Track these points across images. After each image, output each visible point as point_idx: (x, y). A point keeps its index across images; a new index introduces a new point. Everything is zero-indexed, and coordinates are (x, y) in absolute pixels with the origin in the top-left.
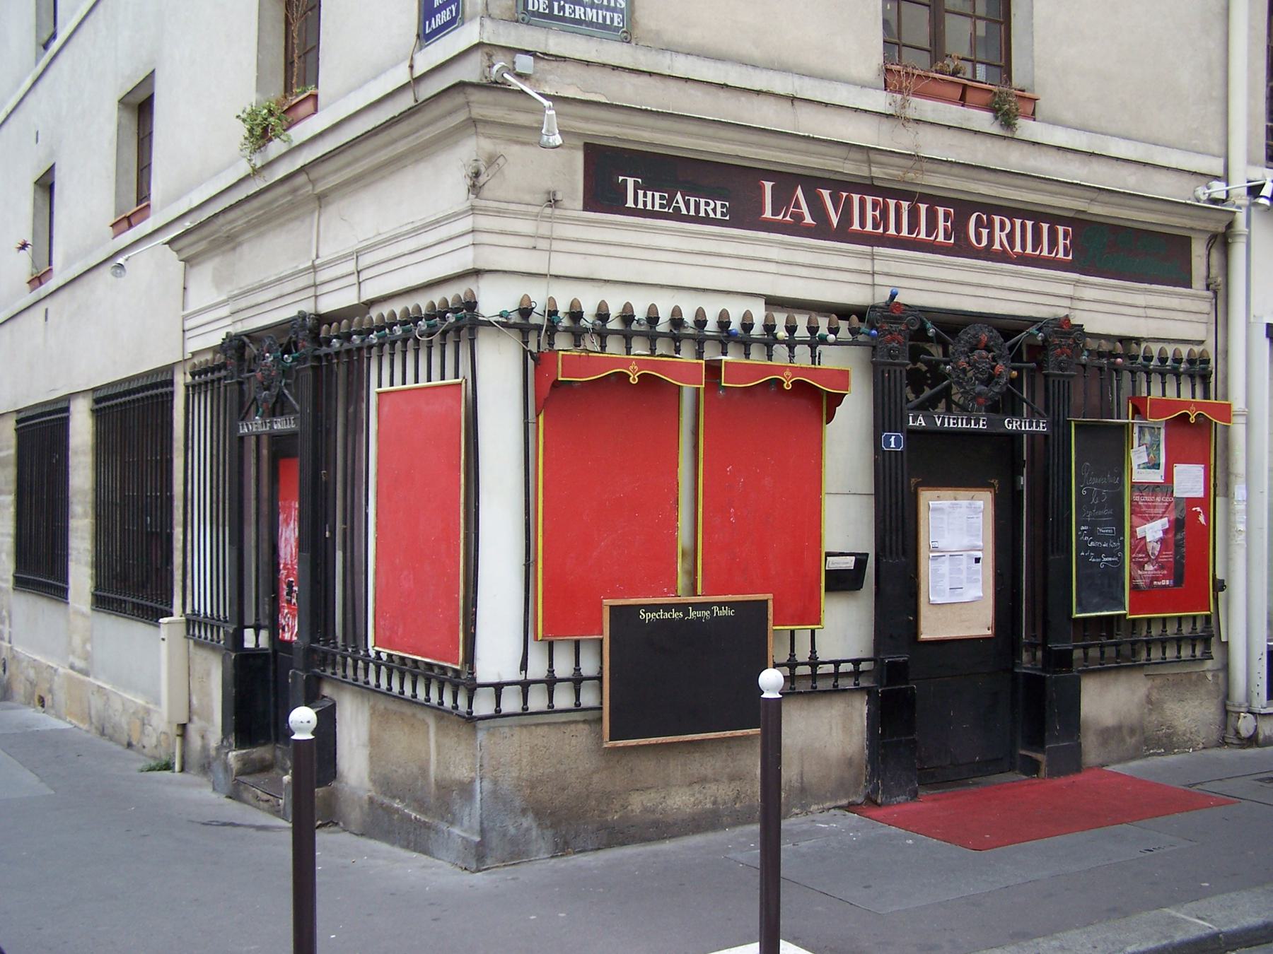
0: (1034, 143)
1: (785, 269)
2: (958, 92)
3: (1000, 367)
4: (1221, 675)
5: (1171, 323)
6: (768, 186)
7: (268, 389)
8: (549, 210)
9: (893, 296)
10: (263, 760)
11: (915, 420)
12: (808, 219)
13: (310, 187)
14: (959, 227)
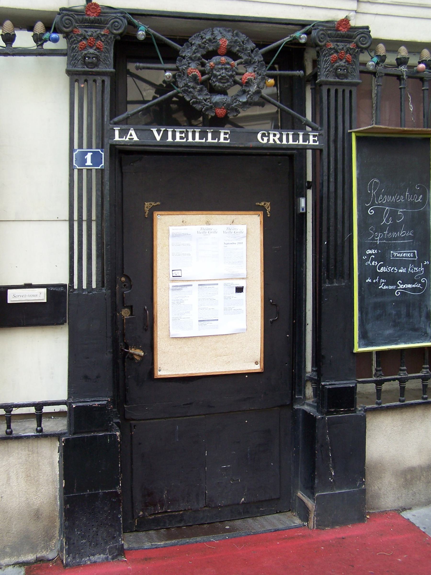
11: (123, 133)
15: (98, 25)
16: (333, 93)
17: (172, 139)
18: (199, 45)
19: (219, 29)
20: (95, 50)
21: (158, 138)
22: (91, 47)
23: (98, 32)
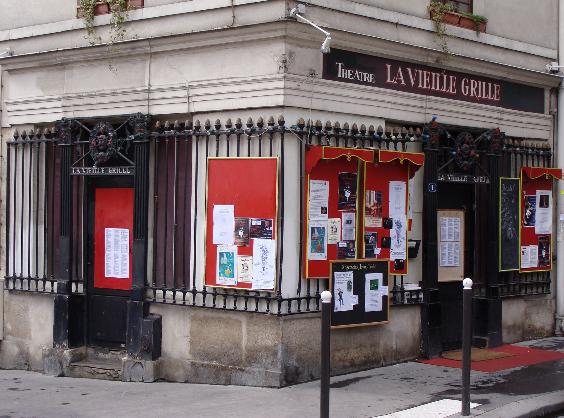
0: (485, 44)
1: (394, 106)
2: (457, 20)
3: (472, 152)
4: (553, 301)
5: (536, 130)
6: (389, 66)
7: (104, 151)
8: (311, 79)
9: (434, 119)
10: (81, 354)
12: (403, 83)
13: (149, 48)
14: (458, 86)
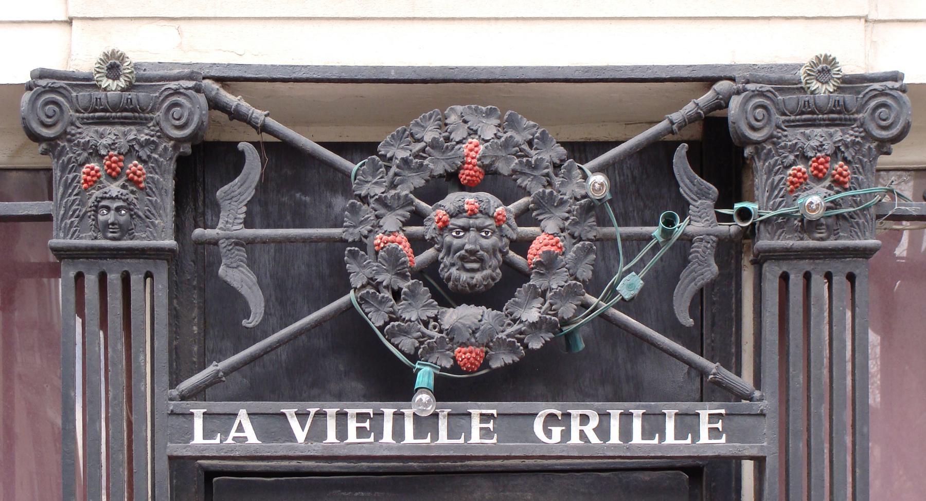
15: (809, 116)
16: (114, 278)
17: (393, 438)
18: (405, 161)
19: (459, 108)
20: (124, 187)
21: (300, 435)
22: (113, 178)
23: (838, 137)
